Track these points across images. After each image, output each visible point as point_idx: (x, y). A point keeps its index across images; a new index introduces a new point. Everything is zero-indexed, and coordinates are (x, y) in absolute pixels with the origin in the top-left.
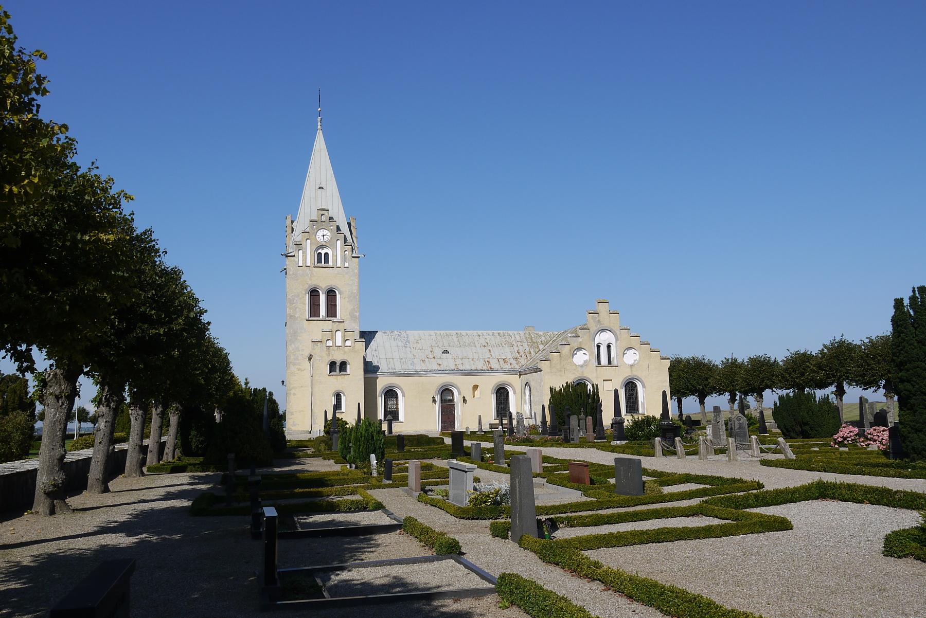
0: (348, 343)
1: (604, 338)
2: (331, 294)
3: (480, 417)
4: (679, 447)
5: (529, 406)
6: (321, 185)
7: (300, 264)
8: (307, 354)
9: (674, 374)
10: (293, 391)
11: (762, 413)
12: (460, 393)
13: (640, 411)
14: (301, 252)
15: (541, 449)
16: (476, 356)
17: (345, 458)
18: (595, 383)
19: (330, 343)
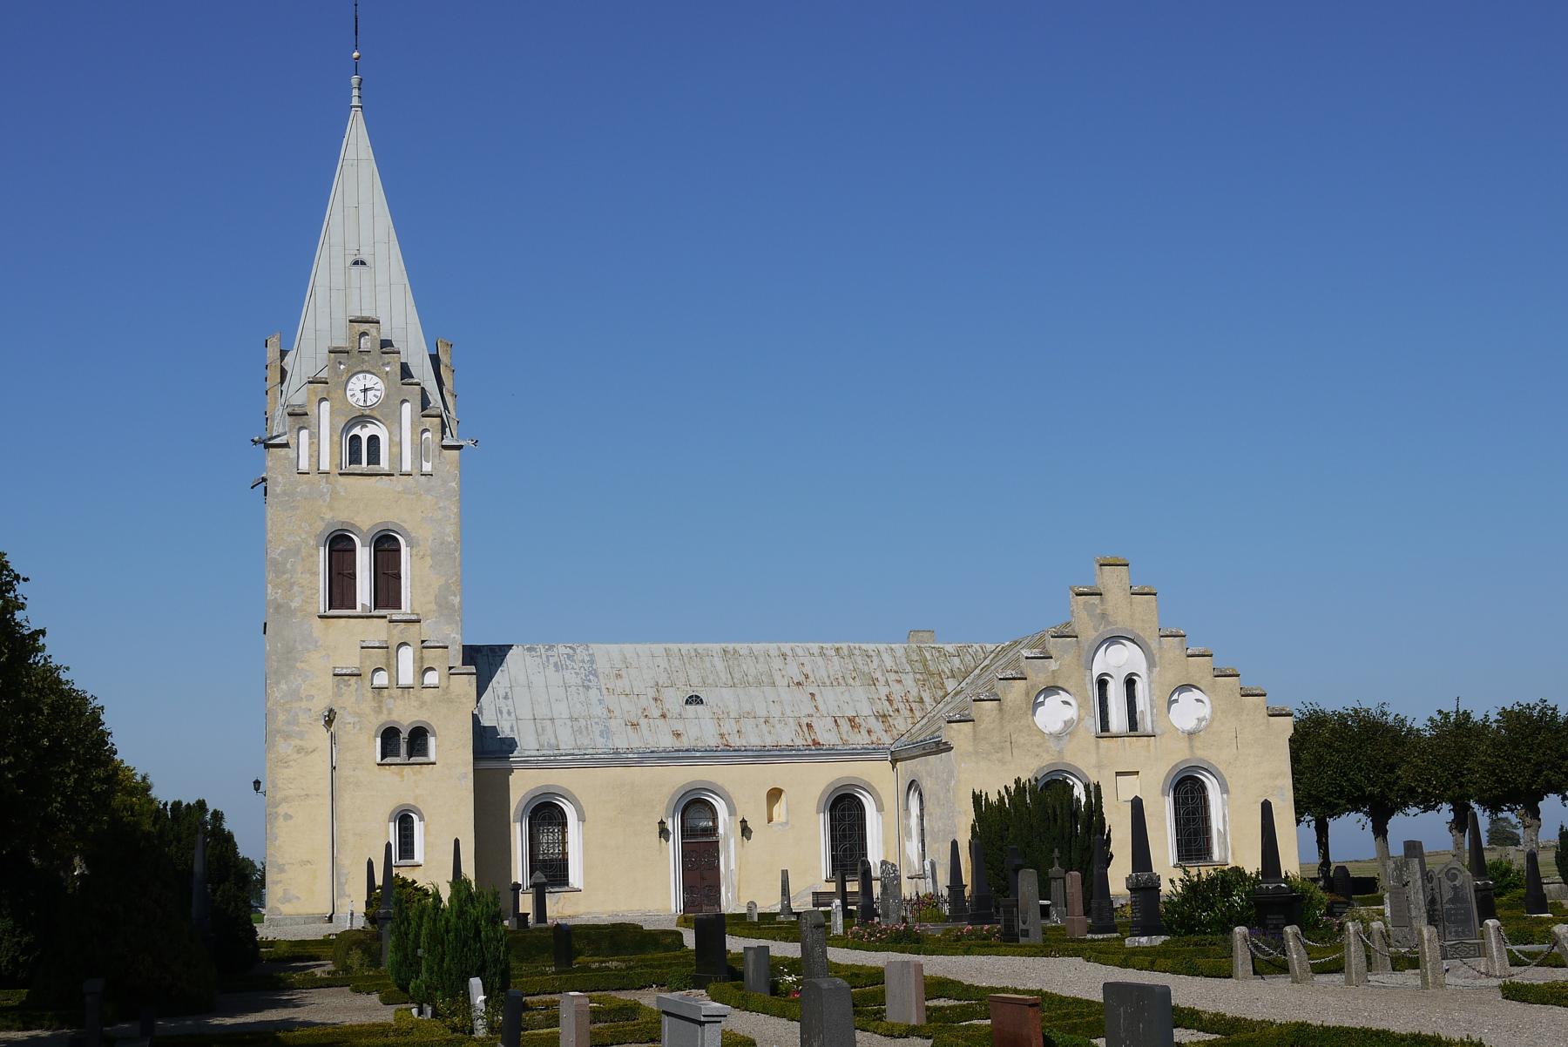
0: (431, 678)
1: (1118, 660)
2: (386, 547)
3: (785, 874)
4: (1295, 953)
5: (914, 846)
6: (359, 259)
7: (304, 465)
8: (320, 706)
9: (1304, 755)
10: (283, 809)
11: (1532, 858)
12: (732, 811)
13: (1216, 855)
14: (304, 434)
15: (921, 958)
16: (775, 711)
17: (405, 989)
18: (1093, 779)
19: (381, 679)
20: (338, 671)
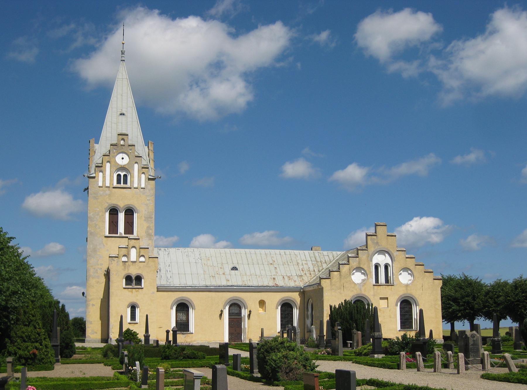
2: (129, 212)
10: (91, 303)
20: (111, 256)
